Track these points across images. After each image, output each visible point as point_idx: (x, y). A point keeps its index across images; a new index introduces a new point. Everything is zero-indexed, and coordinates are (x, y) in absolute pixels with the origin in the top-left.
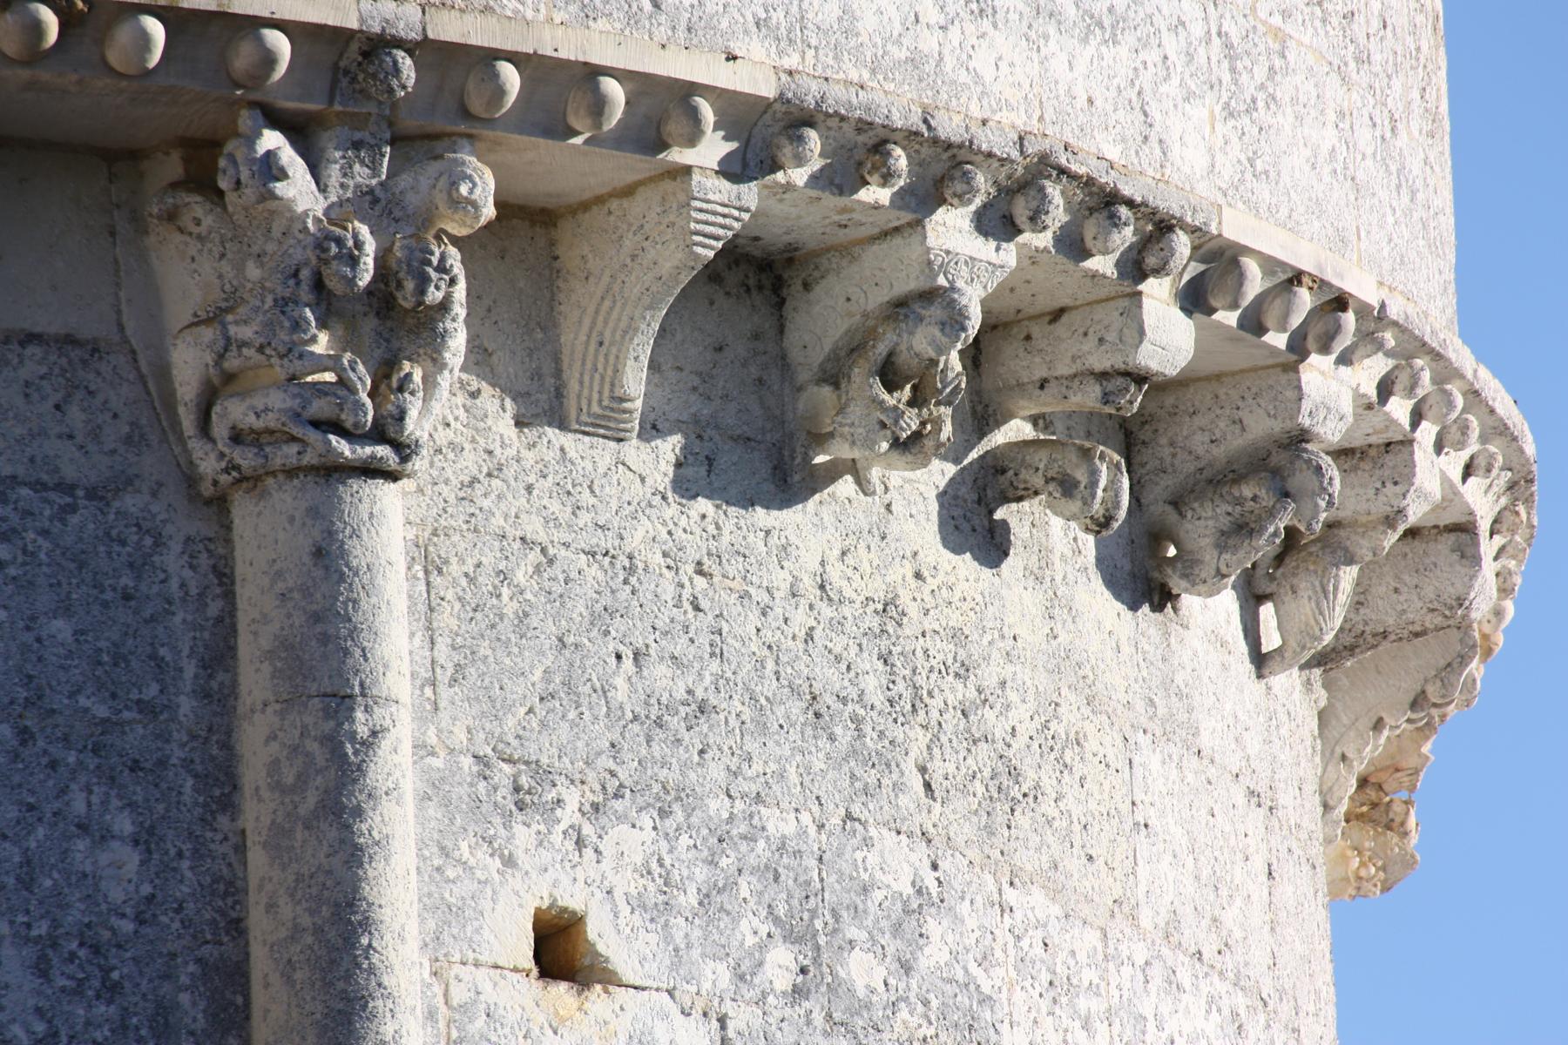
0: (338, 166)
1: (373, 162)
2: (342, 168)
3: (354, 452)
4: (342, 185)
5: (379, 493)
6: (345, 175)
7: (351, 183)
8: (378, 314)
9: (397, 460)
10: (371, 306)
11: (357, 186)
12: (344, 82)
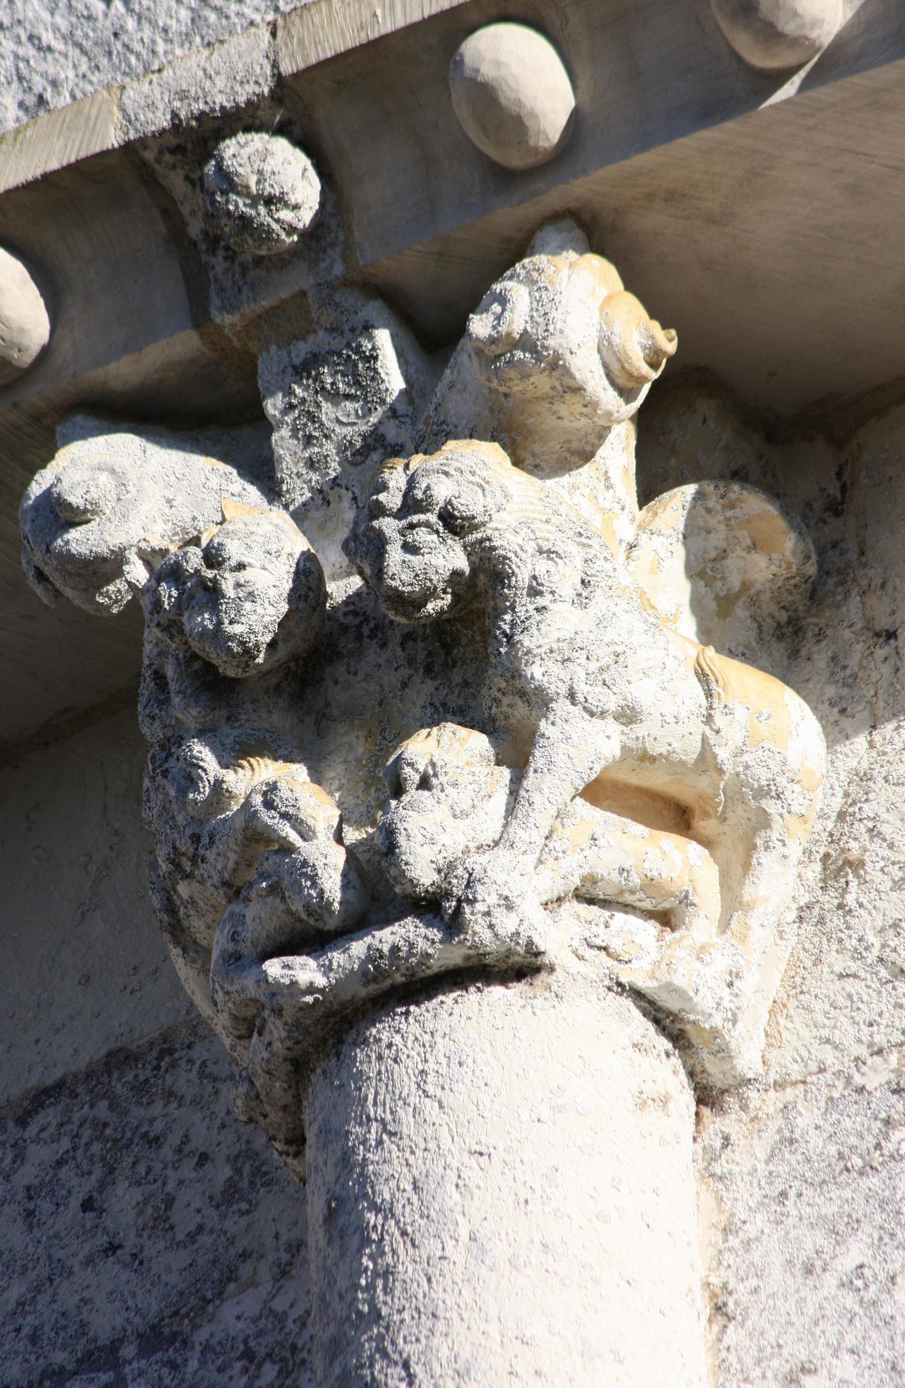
0: (285, 432)
1: (357, 383)
2: (295, 431)
3: (327, 970)
4: (311, 464)
5: (443, 1024)
6: (309, 440)
7: (329, 448)
8: (429, 670)
9: (435, 934)
10: (411, 662)
11: (342, 449)
12: (219, 263)
